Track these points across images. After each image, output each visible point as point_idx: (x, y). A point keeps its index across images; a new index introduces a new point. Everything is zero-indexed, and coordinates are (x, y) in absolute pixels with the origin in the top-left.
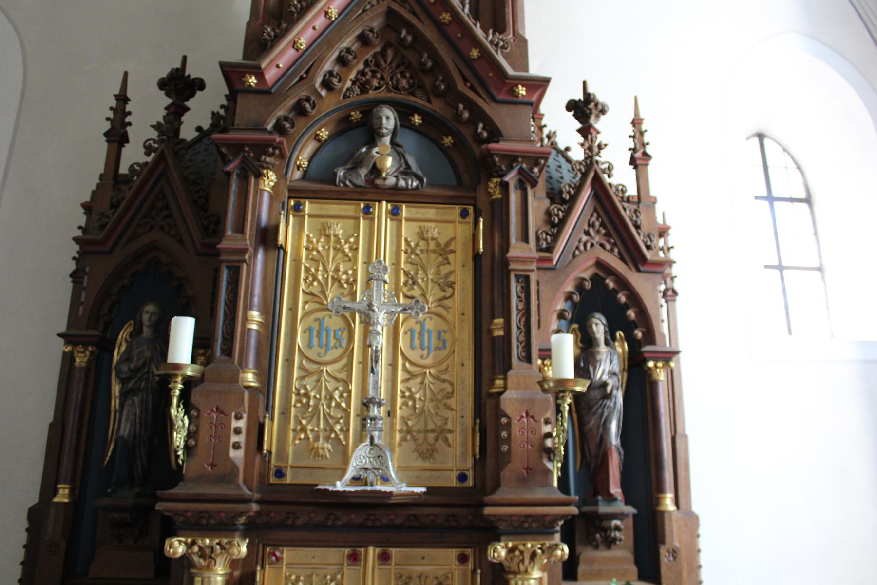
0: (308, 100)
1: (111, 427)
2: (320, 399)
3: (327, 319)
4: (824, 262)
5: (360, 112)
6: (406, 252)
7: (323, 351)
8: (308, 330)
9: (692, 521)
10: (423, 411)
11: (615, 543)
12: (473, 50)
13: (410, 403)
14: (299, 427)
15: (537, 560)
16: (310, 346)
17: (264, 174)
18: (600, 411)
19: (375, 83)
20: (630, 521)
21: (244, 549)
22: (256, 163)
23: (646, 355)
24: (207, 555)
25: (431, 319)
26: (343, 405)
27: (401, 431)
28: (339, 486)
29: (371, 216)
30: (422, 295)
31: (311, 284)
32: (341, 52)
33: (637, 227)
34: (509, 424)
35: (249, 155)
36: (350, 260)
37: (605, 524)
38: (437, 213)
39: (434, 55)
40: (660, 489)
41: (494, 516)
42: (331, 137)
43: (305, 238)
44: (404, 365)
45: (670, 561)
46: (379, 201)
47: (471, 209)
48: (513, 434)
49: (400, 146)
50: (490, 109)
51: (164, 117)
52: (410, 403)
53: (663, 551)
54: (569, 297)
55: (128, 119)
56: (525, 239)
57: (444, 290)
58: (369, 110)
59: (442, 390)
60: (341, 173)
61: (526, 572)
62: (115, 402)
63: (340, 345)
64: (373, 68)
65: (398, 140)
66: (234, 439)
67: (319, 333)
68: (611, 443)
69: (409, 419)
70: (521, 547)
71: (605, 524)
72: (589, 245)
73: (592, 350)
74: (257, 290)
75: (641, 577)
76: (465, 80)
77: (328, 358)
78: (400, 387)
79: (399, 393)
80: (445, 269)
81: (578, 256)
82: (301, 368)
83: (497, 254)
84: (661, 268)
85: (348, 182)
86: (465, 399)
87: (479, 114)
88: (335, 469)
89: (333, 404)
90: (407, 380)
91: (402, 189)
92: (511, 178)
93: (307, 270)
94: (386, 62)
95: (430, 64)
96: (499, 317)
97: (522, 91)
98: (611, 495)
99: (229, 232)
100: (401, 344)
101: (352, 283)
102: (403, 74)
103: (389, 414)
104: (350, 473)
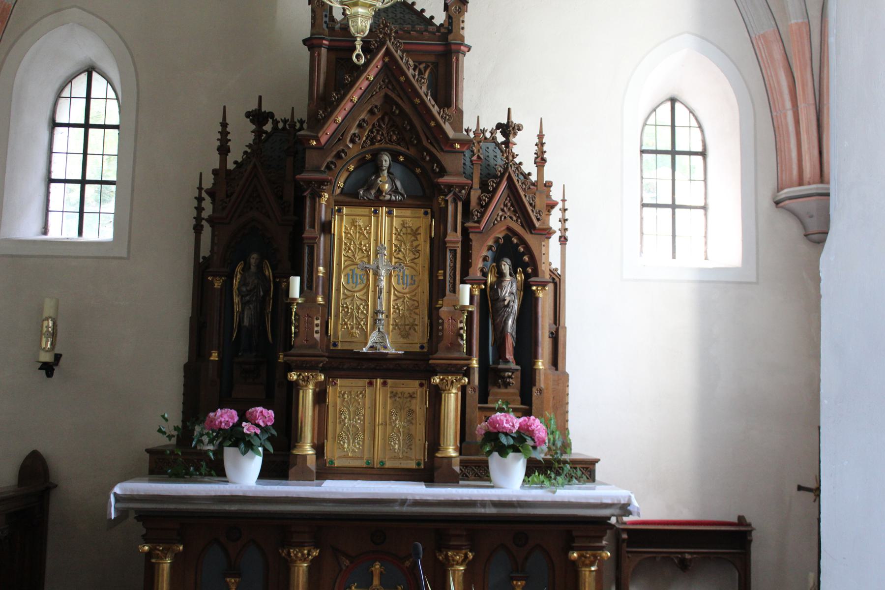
0: (343, 151)
1: (235, 320)
2: (353, 309)
3: (356, 269)
4: (709, 201)
5: (371, 155)
6: (395, 234)
7: (354, 285)
8: (347, 275)
10: (403, 315)
11: (510, 386)
12: (432, 122)
13: (397, 311)
14: (344, 323)
15: (454, 385)
16: (348, 283)
17: (322, 195)
18: (503, 313)
20: (519, 374)
21: (323, 377)
22: (317, 190)
23: (531, 283)
24: (306, 380)
25: (408, 269)
26: (365, 312)
27: (393, 325)
28: (365, 350)
29: (377, 215)
30: (403, 257)
31: (348, 252)
32: (360, 121)
34: (443, 323)
35: (314, 186)
36: (367, 239)
37: (502, 374)
38: (412, 213)
39: (411, 123)
41: (434, 364)
42: (354, 169)
43: (344, 227)
44: (394, 292)
45: (538, 395)
46: (381, 207)
47: (429, 211)
48: (444, 327)
49: (392, 174)
50: (439, 155)
51: (254, 140)
52: (397, 311)
53: (534, 390)
55: (229, 137)
56: (455, 230)
57: (415, 255)
58: (376, 156)
59: (413, 305)
61: (449, 390)
62: (237, 308)
63: (363, 283)
64: (378, 128)
65: (391, 171)
66: (316, 329)
67: (352, 277)
68: (507, 331)
69: (397, 319)
70: (446, 378)
71: (502, 374)
72: (503, 218)
73: (502, 279)
74: (322, 256)
76: (428, 139)
77: (357, 289)
78: (392, 303)
79: (392, 306)
80: (415, 243)
81: (496, 224)
82: (344, 294)
83: (441, 235)
85: (365, 197)
87: (434, 159)
88: (361, 342)
89: (360, 312)
90: (396, 300)
91: (393, 201)
92: (450, 197)
93: (346, 244)
94: (384, 125)
95: (408, 128)
96: (441, 270)
97: (458, 146)
98: (507, 359)
99: (307, 228)
100: (393, 282)
101: (368, 251)
102: (394, 132)
103: (387, 316)
104: (369, 344)
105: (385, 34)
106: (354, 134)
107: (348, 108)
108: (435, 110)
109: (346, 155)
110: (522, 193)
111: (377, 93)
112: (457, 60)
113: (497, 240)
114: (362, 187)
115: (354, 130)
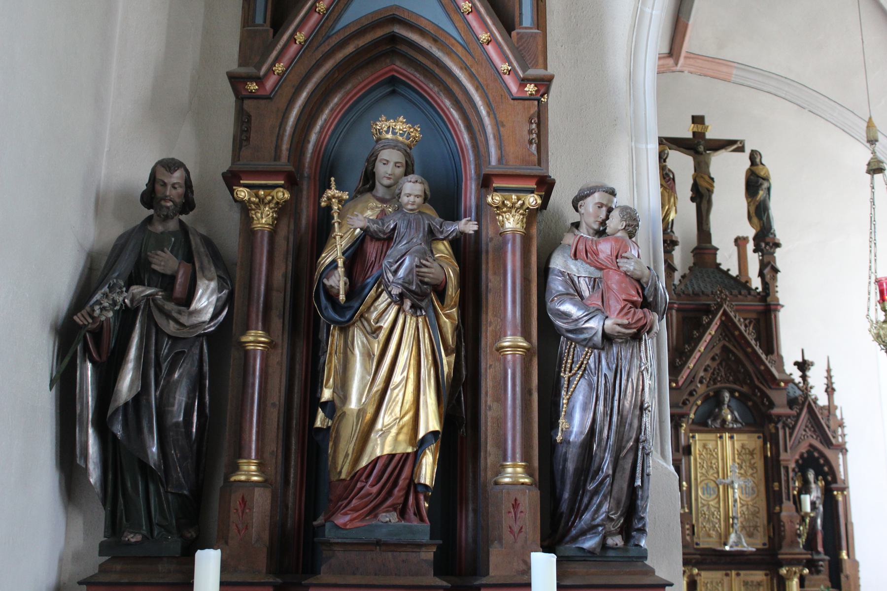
8: (703, 488)
9: (856, 564)
10: (748, 519)
19: (719, 379)
20: (827, 563)
28: (727, 548)
33: (829, 427)
40: (840, 549)
42: (702, 403)
50: (770, 393)
54: (797, 462)
58: (718, 395)
60: (710, 422)
68: (817, 529)
72: (806, 437)
75: (833, 587)
76: (758, 379)
84: (842, 449)
86: (763, 514)
87: (764, 395)
92: (780, 426)
93: (700, 463)
97: (782, 384)
101: (717, 468)
105: (722, 298)
106: (702, 377)
107: (697, 357)
108: (763, 357)
109: (696, 393)
110: (820, 417)
111: (717, 344)
112: (775, 317)
113: (802, 456)
114: (709, 417)
115: (702, 374)
